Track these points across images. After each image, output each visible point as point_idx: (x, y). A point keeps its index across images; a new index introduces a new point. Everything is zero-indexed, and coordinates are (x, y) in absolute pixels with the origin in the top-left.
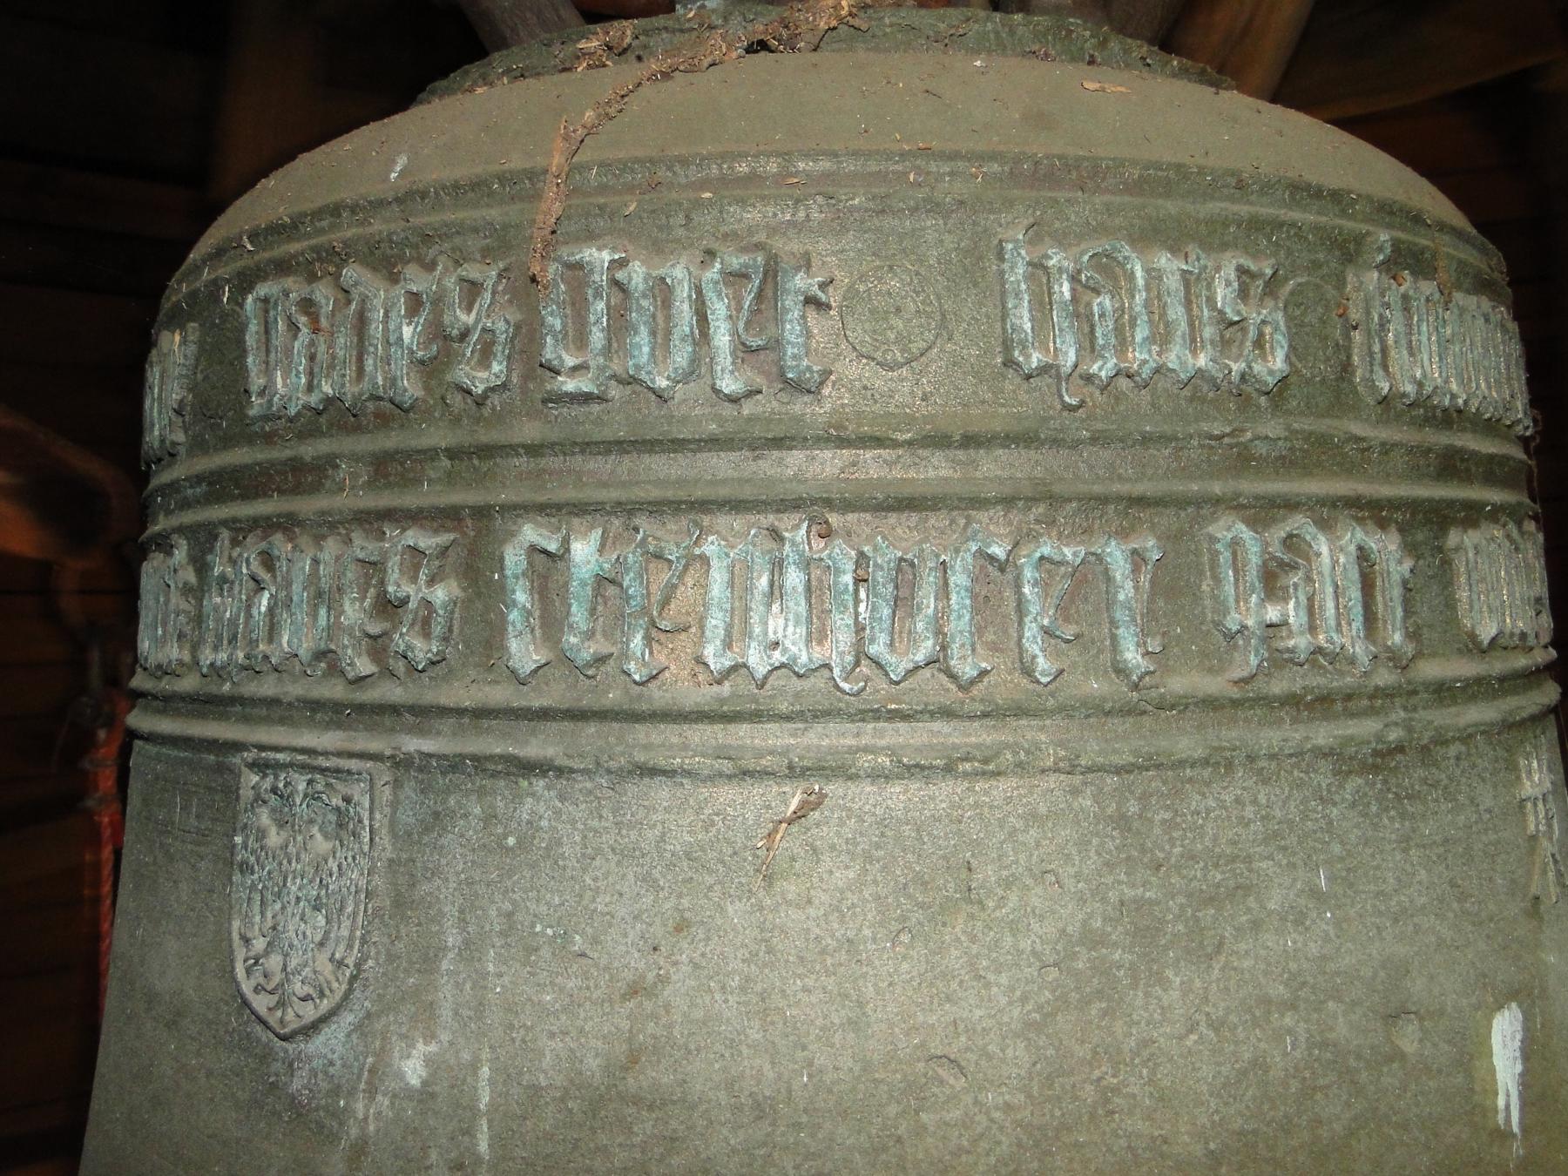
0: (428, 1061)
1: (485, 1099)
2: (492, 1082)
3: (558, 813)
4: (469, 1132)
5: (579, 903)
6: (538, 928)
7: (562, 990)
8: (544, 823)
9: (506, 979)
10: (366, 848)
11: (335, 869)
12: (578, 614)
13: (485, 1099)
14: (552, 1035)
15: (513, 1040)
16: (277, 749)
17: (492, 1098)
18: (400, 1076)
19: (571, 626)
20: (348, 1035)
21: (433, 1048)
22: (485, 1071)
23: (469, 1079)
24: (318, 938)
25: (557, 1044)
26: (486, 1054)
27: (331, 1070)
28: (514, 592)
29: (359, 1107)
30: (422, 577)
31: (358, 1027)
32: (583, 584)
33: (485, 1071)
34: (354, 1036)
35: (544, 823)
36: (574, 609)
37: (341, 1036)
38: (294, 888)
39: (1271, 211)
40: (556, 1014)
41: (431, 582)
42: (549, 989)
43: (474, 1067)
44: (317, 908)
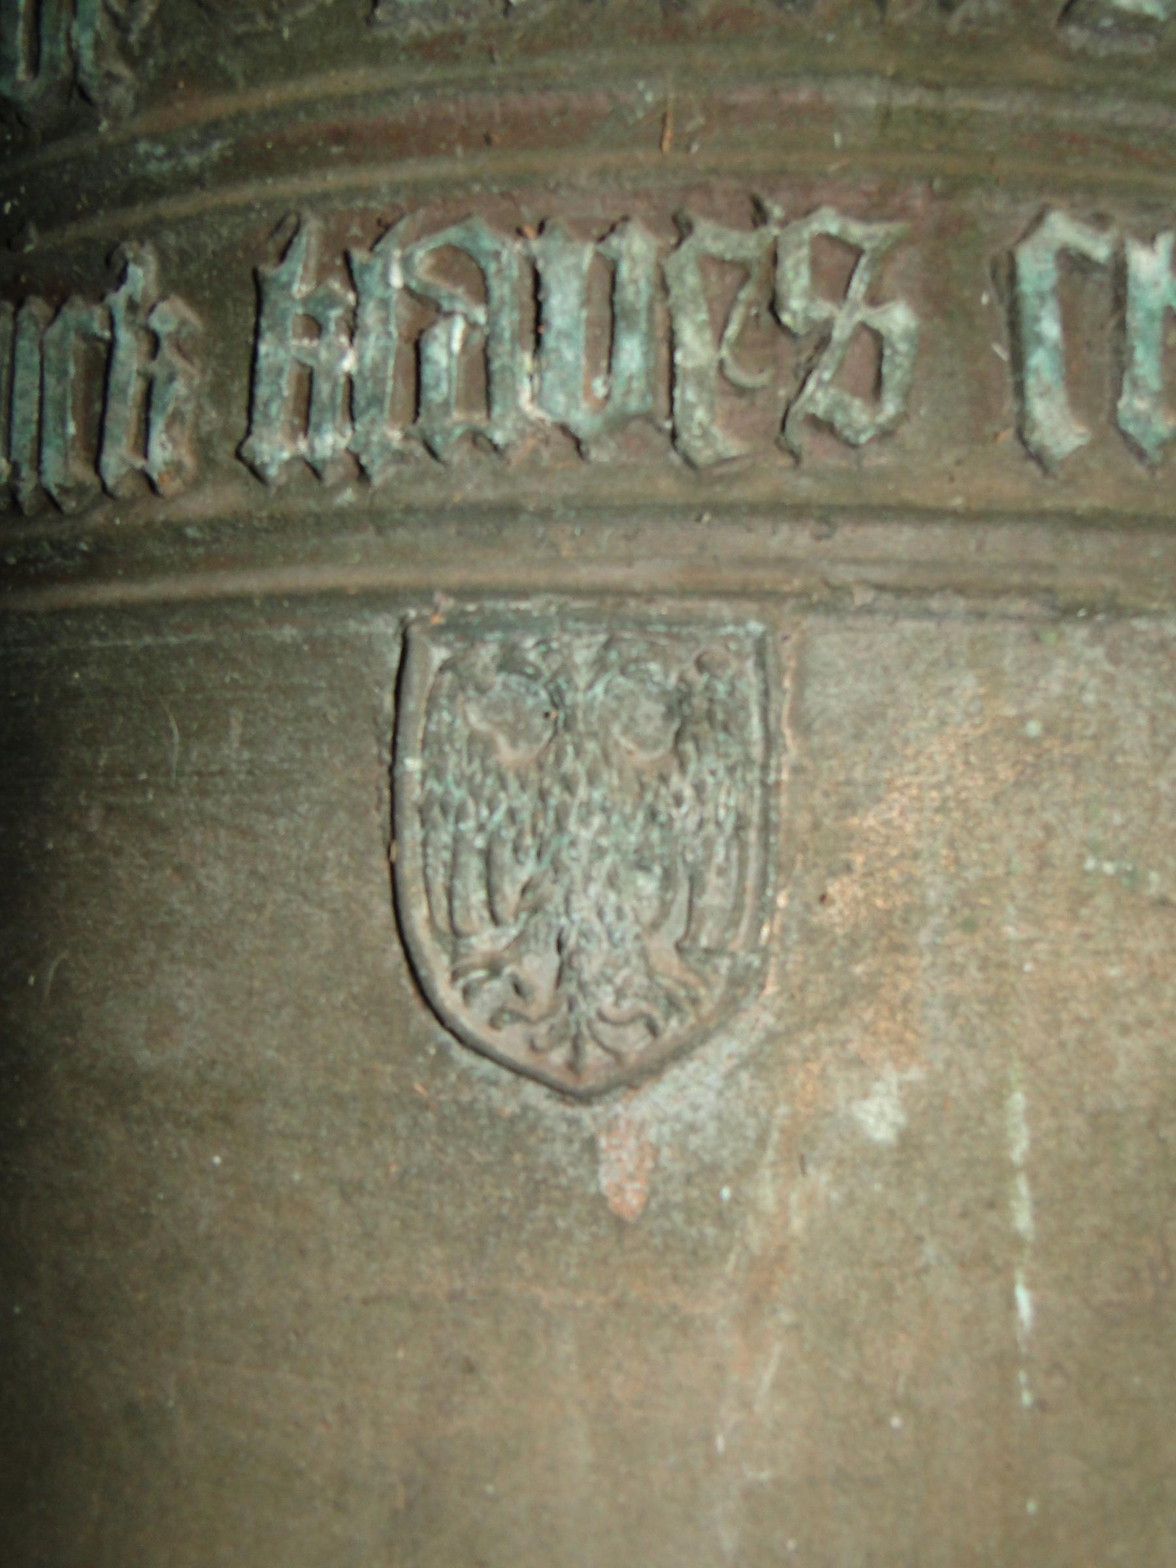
0: (909, 1095)
1: (1019, 1150)
2: (1032, 1115)
3: (1109, 680)
4: (996, 1203)
5: (1152, 821)
6: (1090, 864)
7: (1134, 955)
8: (1090, 698)
9: (1041, 948)
10: (757, 752)
11: (688, 792)
12: (1146, 363)
13: (1019, 1150)
14: (1125, 1030)
15: (1062, 1045)
16: (523, 593)
17: (1034, 1141)
18: (854, 1128)
19: (1135, 383)
20: (730, 1077)
21: (915, 1074)
22: (1018, 1100)
23: (990, 1118)
24: (648, 915)
25: (1136, 1044)
26: (1016, 1071)
27: (694, 1141)
28: (1037, 319)
29: (766, 1194)
30: (858, 287)
31: (755, 1062)
32: (1150, 316)
33: (1018, 1100)
34: (744, 1077)
35: (1090, 698)
36: (1140, 354)
37: (714, 1079)
38: (585, 835)
39: (987, 106)
40: (1129, 993)
41: (874, 299)
42: (1114, 958)
43: (997, 1094)
44: (642, 866)
